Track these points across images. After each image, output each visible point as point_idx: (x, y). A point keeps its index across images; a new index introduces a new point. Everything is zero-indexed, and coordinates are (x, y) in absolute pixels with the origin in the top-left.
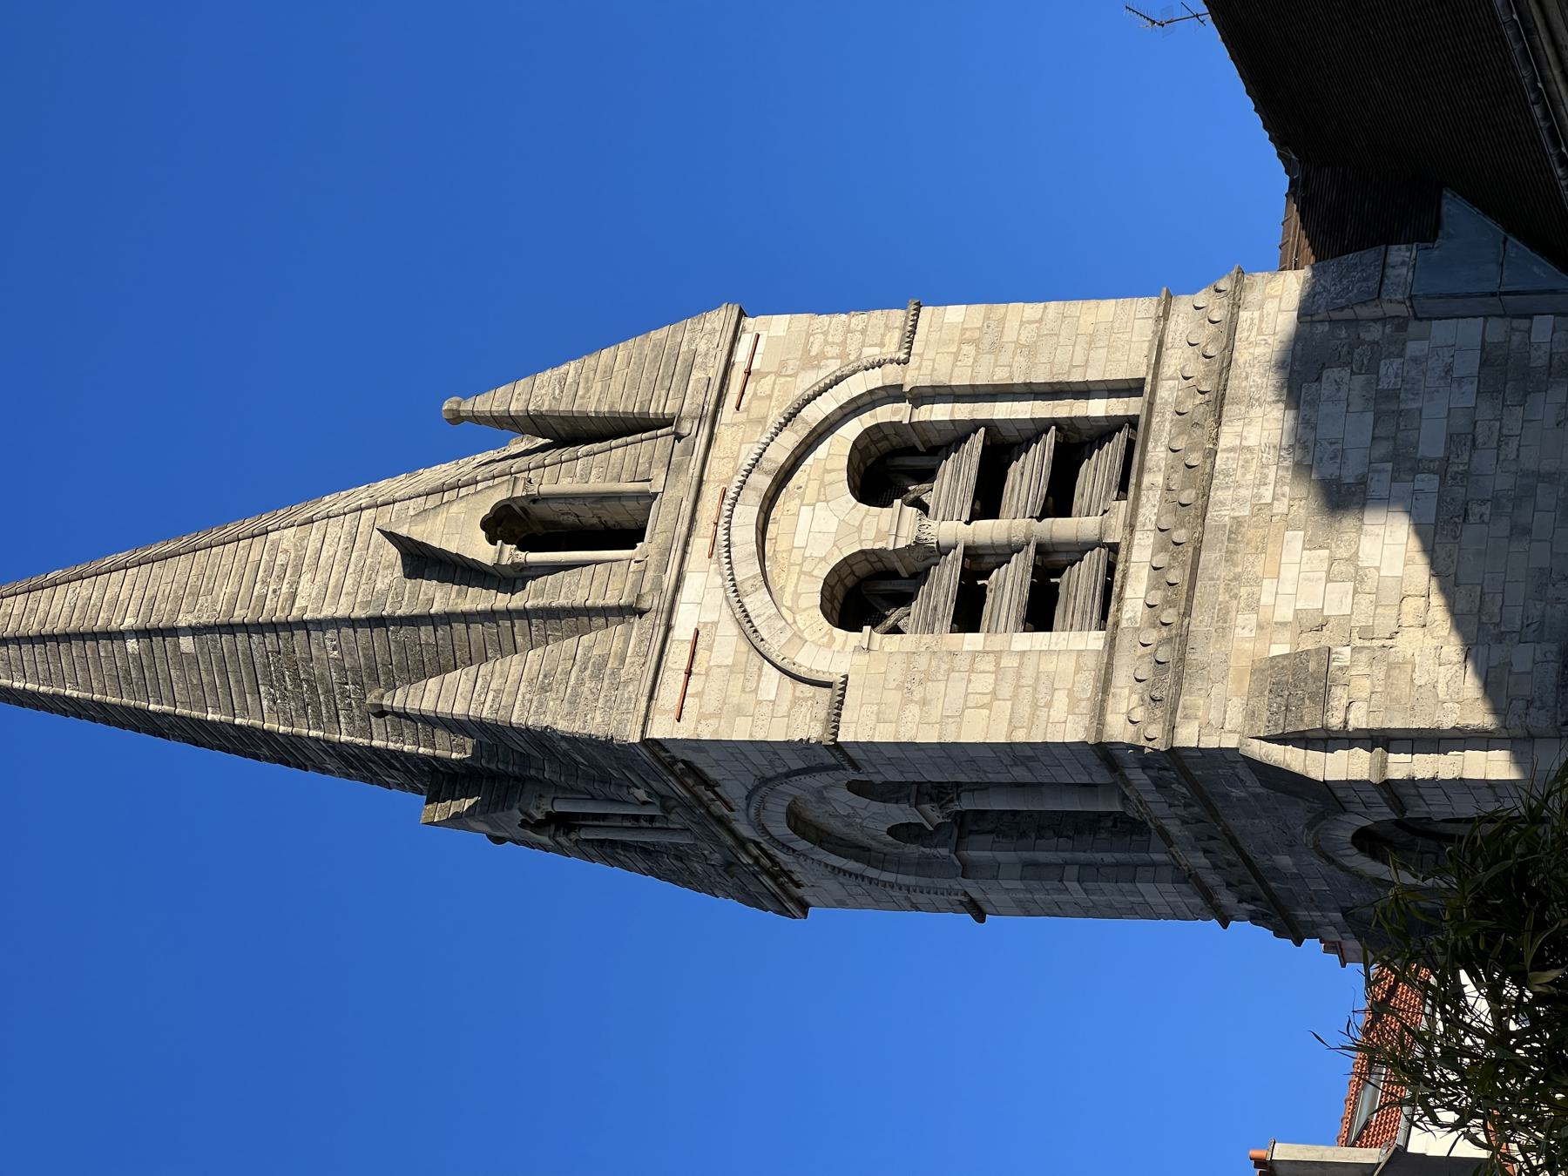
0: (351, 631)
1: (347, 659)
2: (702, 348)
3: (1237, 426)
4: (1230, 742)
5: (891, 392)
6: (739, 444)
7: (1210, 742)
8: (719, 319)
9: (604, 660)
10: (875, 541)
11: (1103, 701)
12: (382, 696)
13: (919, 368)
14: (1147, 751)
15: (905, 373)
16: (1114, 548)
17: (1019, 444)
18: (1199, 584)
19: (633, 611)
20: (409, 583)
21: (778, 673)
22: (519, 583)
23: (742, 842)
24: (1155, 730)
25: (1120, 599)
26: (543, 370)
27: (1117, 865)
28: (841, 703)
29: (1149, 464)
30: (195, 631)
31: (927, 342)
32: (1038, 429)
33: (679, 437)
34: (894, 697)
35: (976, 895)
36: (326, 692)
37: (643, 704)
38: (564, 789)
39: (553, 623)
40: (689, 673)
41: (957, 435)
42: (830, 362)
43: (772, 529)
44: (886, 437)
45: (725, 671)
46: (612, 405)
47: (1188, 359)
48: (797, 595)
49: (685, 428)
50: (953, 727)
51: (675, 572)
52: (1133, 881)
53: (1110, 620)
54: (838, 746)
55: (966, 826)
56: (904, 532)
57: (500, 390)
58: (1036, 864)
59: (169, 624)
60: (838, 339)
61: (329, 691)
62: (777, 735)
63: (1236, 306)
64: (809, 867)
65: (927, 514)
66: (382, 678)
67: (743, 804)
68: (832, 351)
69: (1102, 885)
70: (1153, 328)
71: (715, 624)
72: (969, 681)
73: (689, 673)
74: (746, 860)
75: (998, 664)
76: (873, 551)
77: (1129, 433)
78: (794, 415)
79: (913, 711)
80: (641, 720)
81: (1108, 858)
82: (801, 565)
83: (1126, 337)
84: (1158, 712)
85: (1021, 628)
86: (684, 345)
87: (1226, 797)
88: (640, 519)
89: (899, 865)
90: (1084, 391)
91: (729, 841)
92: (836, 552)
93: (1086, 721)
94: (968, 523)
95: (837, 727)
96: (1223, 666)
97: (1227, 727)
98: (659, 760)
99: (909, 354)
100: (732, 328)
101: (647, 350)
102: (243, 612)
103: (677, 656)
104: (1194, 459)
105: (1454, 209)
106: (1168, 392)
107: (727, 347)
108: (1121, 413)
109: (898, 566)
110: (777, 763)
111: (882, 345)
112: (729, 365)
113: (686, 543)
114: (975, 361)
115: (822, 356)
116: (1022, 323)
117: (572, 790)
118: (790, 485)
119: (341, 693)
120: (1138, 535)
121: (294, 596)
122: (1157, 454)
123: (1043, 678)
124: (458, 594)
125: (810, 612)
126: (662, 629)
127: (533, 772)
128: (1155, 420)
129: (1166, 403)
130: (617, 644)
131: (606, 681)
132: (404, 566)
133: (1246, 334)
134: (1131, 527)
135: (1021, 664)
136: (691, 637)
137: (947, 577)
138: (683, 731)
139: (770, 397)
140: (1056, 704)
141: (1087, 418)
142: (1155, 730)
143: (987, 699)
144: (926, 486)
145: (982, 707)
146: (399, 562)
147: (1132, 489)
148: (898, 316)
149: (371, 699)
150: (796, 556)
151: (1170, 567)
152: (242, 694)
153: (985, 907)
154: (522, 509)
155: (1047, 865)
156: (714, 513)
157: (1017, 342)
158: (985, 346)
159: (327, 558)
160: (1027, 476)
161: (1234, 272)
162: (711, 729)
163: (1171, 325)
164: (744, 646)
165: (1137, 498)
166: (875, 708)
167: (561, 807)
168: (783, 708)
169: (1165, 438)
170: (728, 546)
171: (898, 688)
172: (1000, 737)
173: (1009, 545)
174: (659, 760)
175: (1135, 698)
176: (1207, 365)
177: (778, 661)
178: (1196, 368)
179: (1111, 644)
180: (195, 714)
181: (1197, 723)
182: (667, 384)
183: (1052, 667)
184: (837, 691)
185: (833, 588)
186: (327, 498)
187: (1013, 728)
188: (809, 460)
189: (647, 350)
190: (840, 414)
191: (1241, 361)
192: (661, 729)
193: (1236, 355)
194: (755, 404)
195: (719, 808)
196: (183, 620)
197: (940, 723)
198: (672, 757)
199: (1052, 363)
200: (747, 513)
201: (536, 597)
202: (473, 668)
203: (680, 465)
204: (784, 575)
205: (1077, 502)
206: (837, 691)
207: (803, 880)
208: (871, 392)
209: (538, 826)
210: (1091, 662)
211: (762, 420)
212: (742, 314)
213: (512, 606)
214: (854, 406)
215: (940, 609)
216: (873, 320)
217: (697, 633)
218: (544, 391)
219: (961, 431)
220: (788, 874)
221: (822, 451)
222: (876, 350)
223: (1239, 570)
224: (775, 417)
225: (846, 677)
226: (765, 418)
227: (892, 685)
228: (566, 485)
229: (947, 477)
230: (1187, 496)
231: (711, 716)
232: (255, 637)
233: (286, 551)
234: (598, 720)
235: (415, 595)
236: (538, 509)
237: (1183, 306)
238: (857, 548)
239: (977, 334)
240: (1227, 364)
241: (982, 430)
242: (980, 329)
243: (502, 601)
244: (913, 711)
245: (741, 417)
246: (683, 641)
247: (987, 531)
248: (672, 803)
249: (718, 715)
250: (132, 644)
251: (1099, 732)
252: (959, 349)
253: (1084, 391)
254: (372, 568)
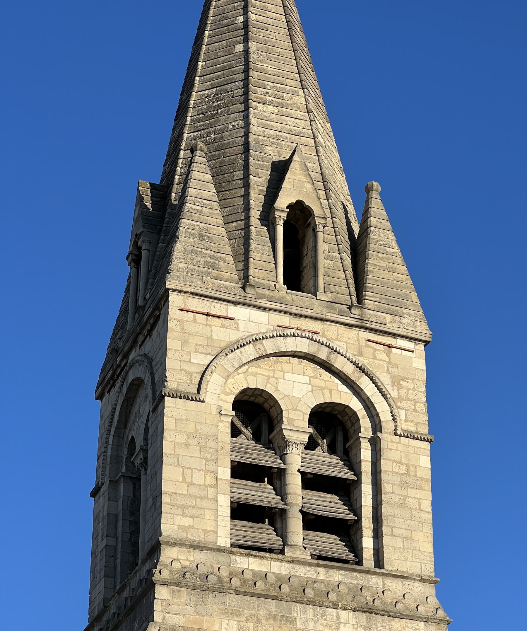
0: (242, 134)
1: (228, 133)
2: (405, 320)
3: (353, 621)
4: (157, 617)
5: (378, 427)
6: (346, 342)
7: (158, 605)
8: (423, 330)
9: (218, 269)
10: (288, 418)
11: (186, 545)
12: (202, 151)
13: (392, 441)
14: (154, 570)
15: (390, 433)
16: (282, 552)
17: (349, 501)
18: (255, 599)
19: (245, 281)
20: (269, 164)
21: (207, 364)
22: (266, 223)
23: (126, 356)
24: (165, 574)
25: (248, 555)
26: (395, 235)
27: (115, 567)
28: (188, 399)
29: (331, 571)
30: (246, 52)
31: (408, 446)
32: (356, 509)
33: (350, 308)
34: (191, 428)
35: (102, 490)
36: (211, 124)
37: (189, 290)
38: (154, 255)
39: (242, 241)
40: (208, 315)
41: (353, 465)
42: (396, 392)
43: (295, 361)
44: (353, 425)
45: (209, 335)
46: (372, 272)
47: (395, 593)
48: (255, 375)
49: (356, 311)
50: (172, 461)
51: (268, 306)
52: (106, 576)
53: (235, 549)
54: (162, 397)
56: (293, 434)
57: (384, 213)
58: (117, 522)
59: (250, 37)
60: (410, 396)
61: (211, 125)
62: (169, 364)
63: (427, 620)
64: (116, 396)
65: (305, 448)
66: (217, 153)
67: (142, 353)
68: (403, 393)
69: (104, 559)
70: (415, 574)
71: (237, 329)
72: (200, 470)
73: (208, 315)
74: (119, 359)
75: (210, 486)
76: (282, 417)
78: (363, 372)
79: (182, 439)
80: (180, 288)
81: (119, 561)
82: (273, 377)
83: (410, 558)
84: (177, 576)
85: (233, 500)
86: (408, 311)
87: (134, 620)
88: (305, 290)
89: (117, 446)
90: (377, 535)
91: (126, 349)
92: (281, 397)
93: (174, 536)
94: (299, 471)
95: (173, 397)
96: (204, 613)
97: (167, 615)
98: (159, 301)
99: (400, 436)
100: (417, 337)
101: (405, 291)
102: (256, 76)
103: (218, 308)
104: (333, 597)
106: (376, 582)
107: (405, 334)
108: (364, 556)
109: (275, 432)
110: (157, 367)
111: (406, 421)
112: (394, 335)
113: (286, 313)
114: (396, 473)
115: (400, 387)
116: (419, 499)
117: (153, 260)
118: (322, 371)
119: (209, 132)
120: (287, 565)
121: (264, 103)
122: (337, 576)
123: (201, 512)
124: (262, 191)
125: (245, 382)
126: (234, 299)
127: (162, 237)
128: (358, 575)
129: (368, 581)
130: (226, 275)
131: (204, 270)
132: (279, 162)
133: (410, 625)
134: (292, 561)
135: (209, 499)
136: (230, 315)
137: (267, 459)
138: (173, 312)
139: (375, 358)
140: (185, 519)
141: (362, 537)
142: (165, 574)
143: (188, 480)
144: (326, 449)
145: (184, 477)
146: (282, 159)
147: (316, 561)
148: (424, 429)
149: (200, 145)
150: (278, 374)
151: (266, 583)
152: (211, 80)
153: (97, 496)
154: (310, 223)
155: (116, 528)
156: (304, 328)
157: (407, 496)
158: (405, 479)
159: (290, 122)
160: (329, 505)
161: (448, 618)
162: (174, 327)
163: (417, 584)
164: (223, 345)
165: (310, 564)
166: (184, 418)
167: (144, 254)
168: (185, 367)
169: (347, 580)
170: (284, 336)
171: (196, 431)
172: (165, 487)
173: (286, 494)
174: (159, 301)
175: (187, 563)
176: (391, 604)
177: (214, 363)
178: (389, 597)
179: (221, 550)
180: (202, 56)
181: (170, 598)
182: (383, 301)
183: (207, 516)
184: (195, 397)
185: (261, 395)
186: (328, 125)
187: (170, 495)
188: (337, 381)
189: (405, 291)
190: (365, 398)
191: (393, 623)
192: (174, 300)
193: (397, 620)
194: (371, 350)
195: (141, 338)
196: (252, 45)
197: (175, 454)
198: (162, 309)
199: (394, 516)
201: (257, 232)
202: (216, 199)
203: (333, 308)
204: (267, 367)
205: (313, 534)
206: (195, 397)
207: (111, 394)
208: (377, 414)
209: (136, 244)
210: (210, 538)
211: (360, 354)
212: (426, 343)
213: (252, 219)
214: (370, 406)
215: (247, 456)
216: (422, 416)
217: (232, 319)
218: (383, 236)
219: (356, 467)
220: (113, 385)
221: (343, 388)
222: (403, 417)
223: (264, 622)
224: (362, 361)
225: (203, 402)
226: (362, 356)
227: (198, 427)
228: (323, 247)
229: (329, 460)
230: (310, 593)
231: (182, 328)
232: (242, 83)
233: (291, 99)
234: (181, 265)
235: (261, 167)
236: (310, 232)
237: (429, 590)
238: (283, 408)
239: (412, 474)
240: (391, 615)
241: (355, 478)
242: (416, 476)
243: (255, 213)
244: (182, 439)
245: (363, 342)
246: (227, 311)
247: (294, 482)
248: (141, 313)
249: (183, 331)
250: (241, 19)
251: (167, 543)
252: (403, 464)
253: (377, 535)
254: (279, 144)
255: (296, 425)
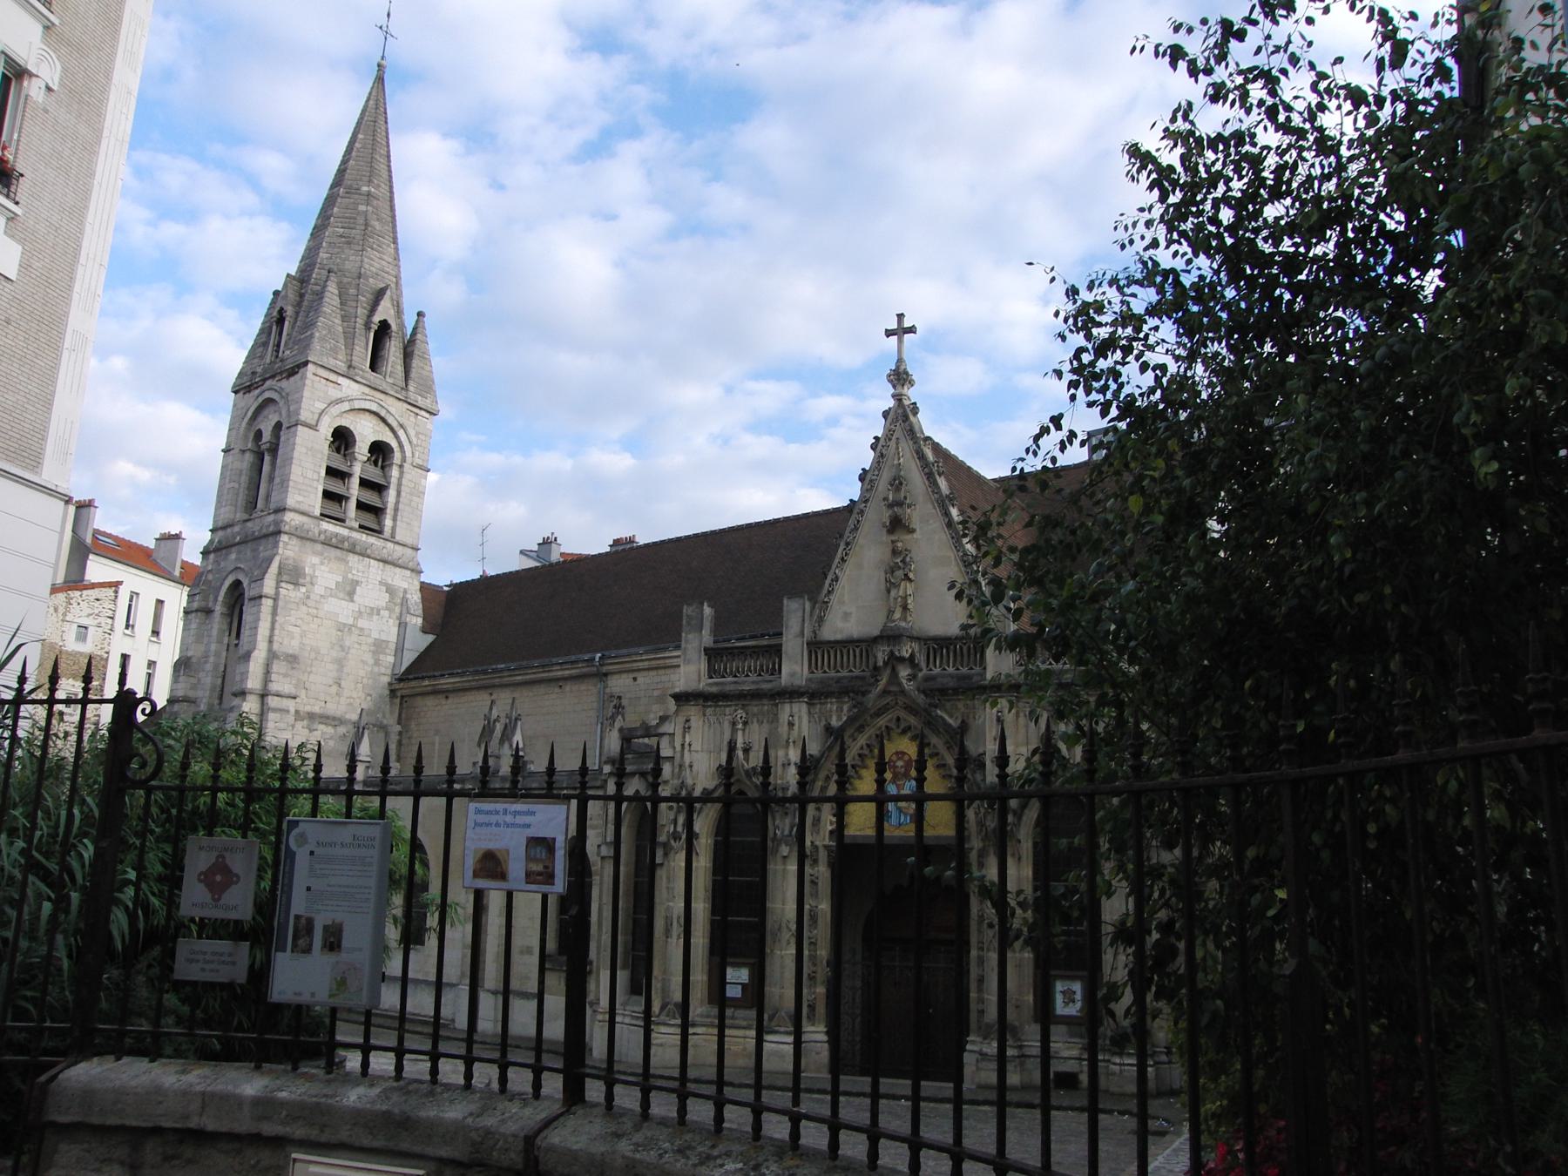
23: (265, 380)
55: (260, 457)
64: (252, 401)
77: (378, 532)
90: (395, 519)
105: (430, 638)
160: (370, 498)
200: (374, 407)
255: (362, 449)
